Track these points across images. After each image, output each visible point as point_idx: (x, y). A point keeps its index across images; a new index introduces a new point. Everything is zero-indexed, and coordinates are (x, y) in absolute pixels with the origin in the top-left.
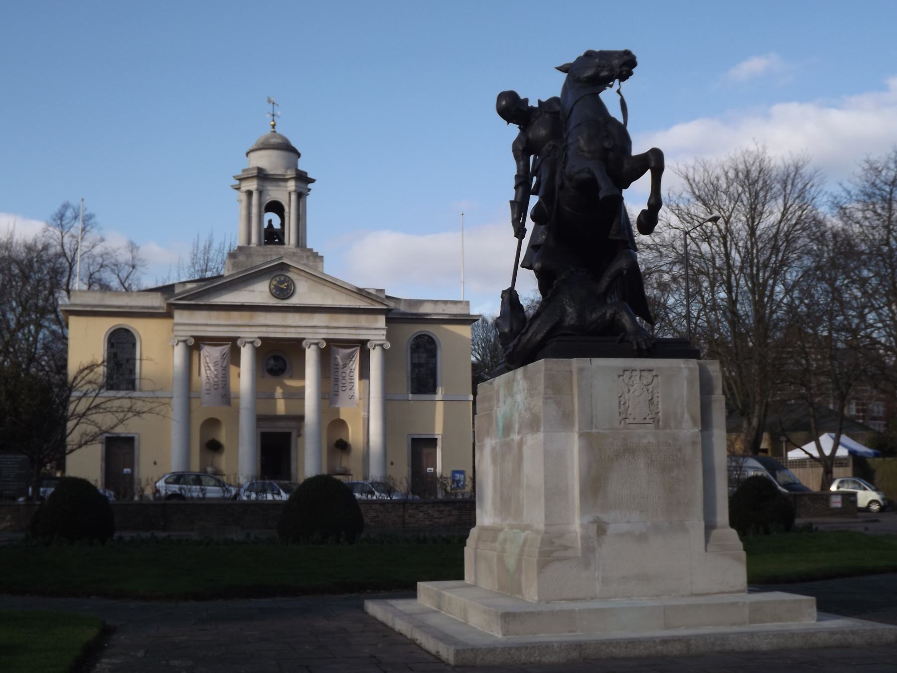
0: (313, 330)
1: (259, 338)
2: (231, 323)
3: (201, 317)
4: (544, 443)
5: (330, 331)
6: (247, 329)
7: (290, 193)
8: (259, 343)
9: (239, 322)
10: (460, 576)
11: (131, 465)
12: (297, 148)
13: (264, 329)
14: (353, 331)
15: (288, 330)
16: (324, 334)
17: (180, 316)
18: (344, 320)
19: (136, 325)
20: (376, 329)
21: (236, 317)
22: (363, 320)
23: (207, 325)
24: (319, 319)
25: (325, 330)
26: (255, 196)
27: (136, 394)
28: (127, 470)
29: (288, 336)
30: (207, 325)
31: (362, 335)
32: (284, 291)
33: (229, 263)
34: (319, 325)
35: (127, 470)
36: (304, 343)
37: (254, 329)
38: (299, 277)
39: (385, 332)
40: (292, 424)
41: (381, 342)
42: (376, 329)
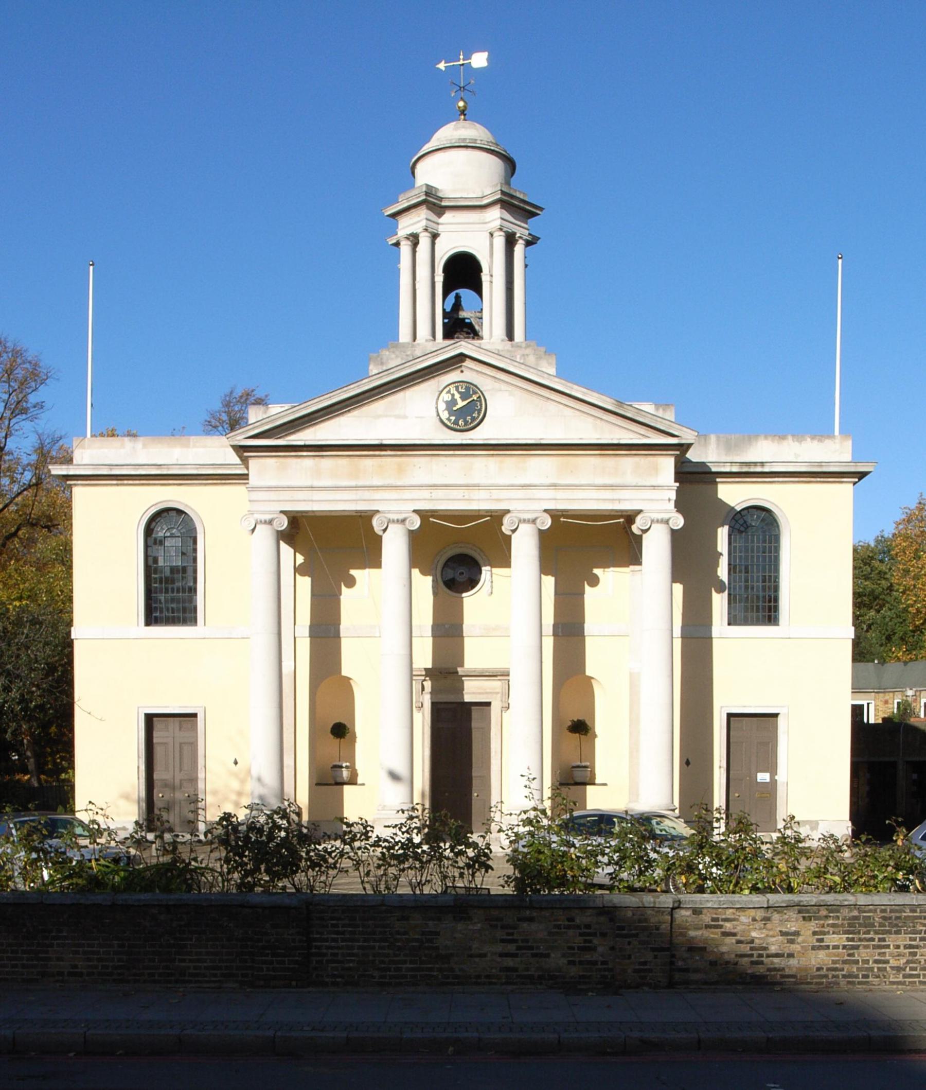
3: (301, 469)
4: (94, 904)
5: (560, 494)
6: (520, 494)
7: (491, 235)
8: (547, 523)
11: (772, 768)
13: (425, 494)
14: (608, 494)
17: (263, 469)
18: (590, 467)
20: (654, 487)
25: (550, 493)
26: (425, 241)
28: (763, 777)
32: (469, 411)
33: (385, 358)
34: (583, 482)
35: (763, 777)
36: (506, 520)
37: (407, 494)
38: (497, 385)
39: (673, 495)
41: (666, 516)
42: (654, 487)
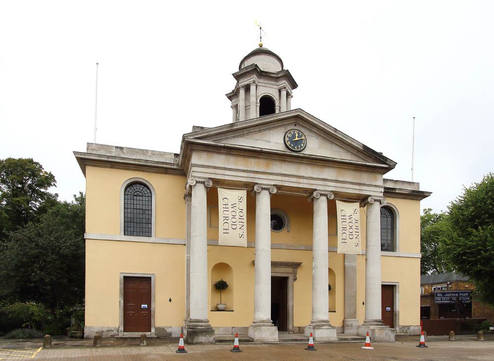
0: (323, 181)
1: (274, 185)
2: (246, 169)
3: (219, 160)
9: (256, 169)
10: (148, 233)
12: (282, 60)
13: (279, 178)
15: (302, 180)
16: (332, 187)
19: (155, 181)
20: (376, 186)
21: (253, 164)
22: (365, 178)
23: (225, 169)
24: (329, 173)
27: (152, 240)
28: (144, 306)
29: (301, 186)
30: (225, 169)
31: (365, 191)
34: (329, 178)
35: (144, 306)
37: (271, 177)
40: (290, 270)
42: (376, 186)
